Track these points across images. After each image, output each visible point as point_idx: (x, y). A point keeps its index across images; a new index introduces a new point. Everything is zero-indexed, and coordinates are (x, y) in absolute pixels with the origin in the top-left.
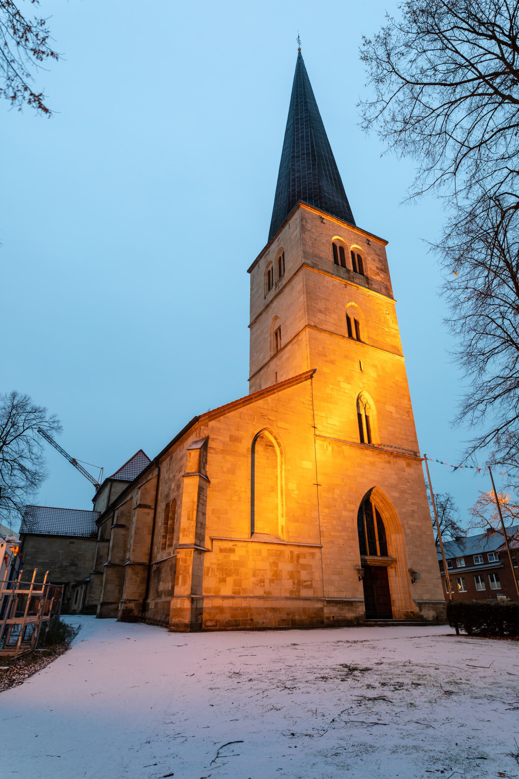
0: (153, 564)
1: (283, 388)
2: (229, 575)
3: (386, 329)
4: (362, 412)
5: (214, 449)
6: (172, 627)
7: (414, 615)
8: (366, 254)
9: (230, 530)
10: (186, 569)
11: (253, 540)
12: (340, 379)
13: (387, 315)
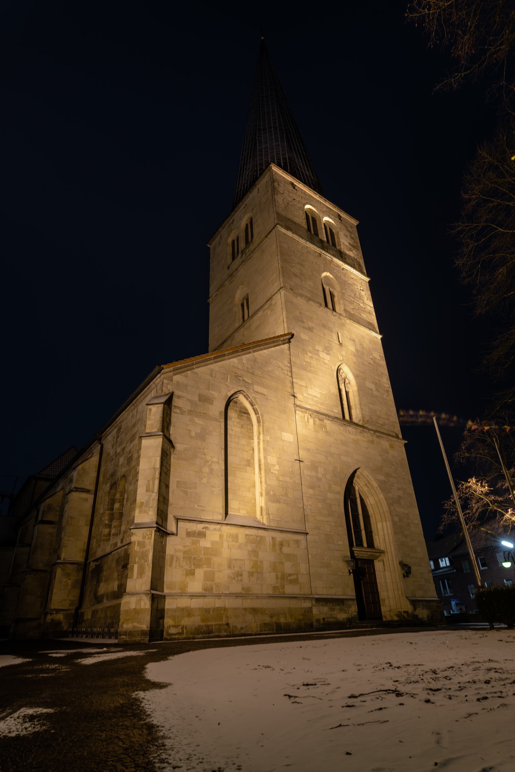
0: (90, 562)
1: (259, 348)
2: (199, 566)
3: (361, 305)
4: (342, 387)
5: (179, 408)
6: (122, 637)
7: (408, 615)
8: (338, 228)
9: (200, 508)
10: (144, 556)
11: (228, 523)
12: (319, 348)
13: (361, 291)
